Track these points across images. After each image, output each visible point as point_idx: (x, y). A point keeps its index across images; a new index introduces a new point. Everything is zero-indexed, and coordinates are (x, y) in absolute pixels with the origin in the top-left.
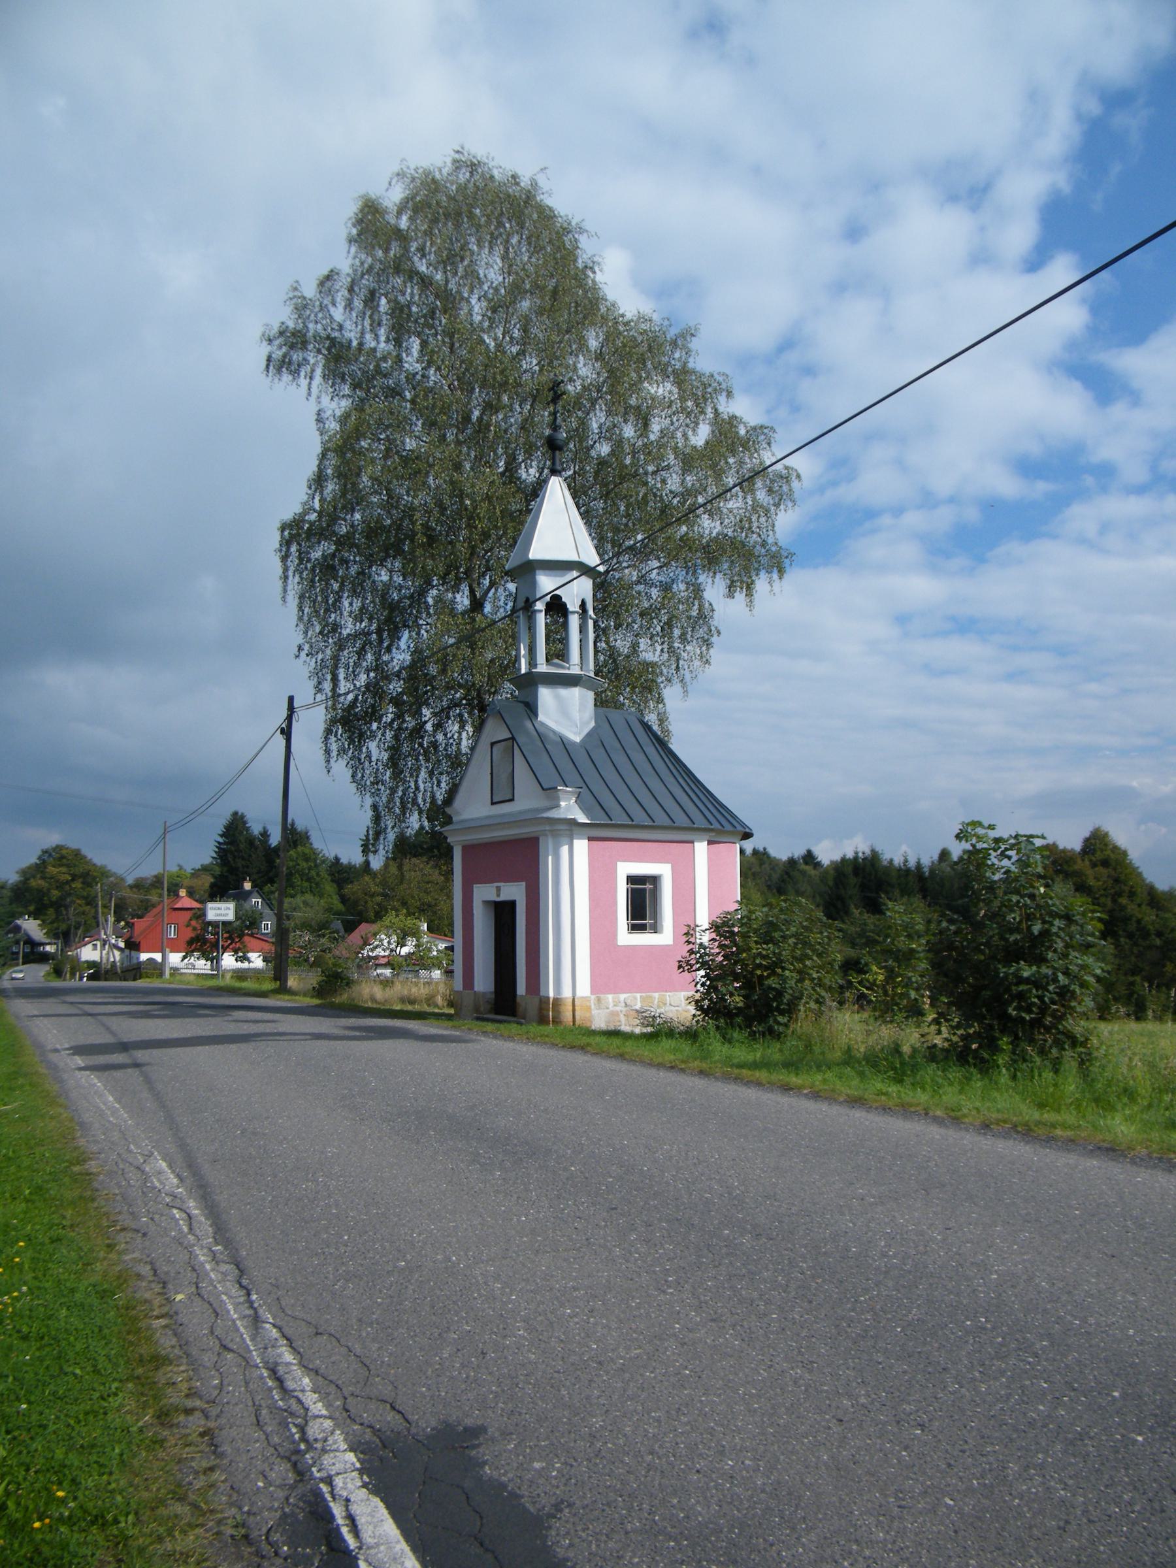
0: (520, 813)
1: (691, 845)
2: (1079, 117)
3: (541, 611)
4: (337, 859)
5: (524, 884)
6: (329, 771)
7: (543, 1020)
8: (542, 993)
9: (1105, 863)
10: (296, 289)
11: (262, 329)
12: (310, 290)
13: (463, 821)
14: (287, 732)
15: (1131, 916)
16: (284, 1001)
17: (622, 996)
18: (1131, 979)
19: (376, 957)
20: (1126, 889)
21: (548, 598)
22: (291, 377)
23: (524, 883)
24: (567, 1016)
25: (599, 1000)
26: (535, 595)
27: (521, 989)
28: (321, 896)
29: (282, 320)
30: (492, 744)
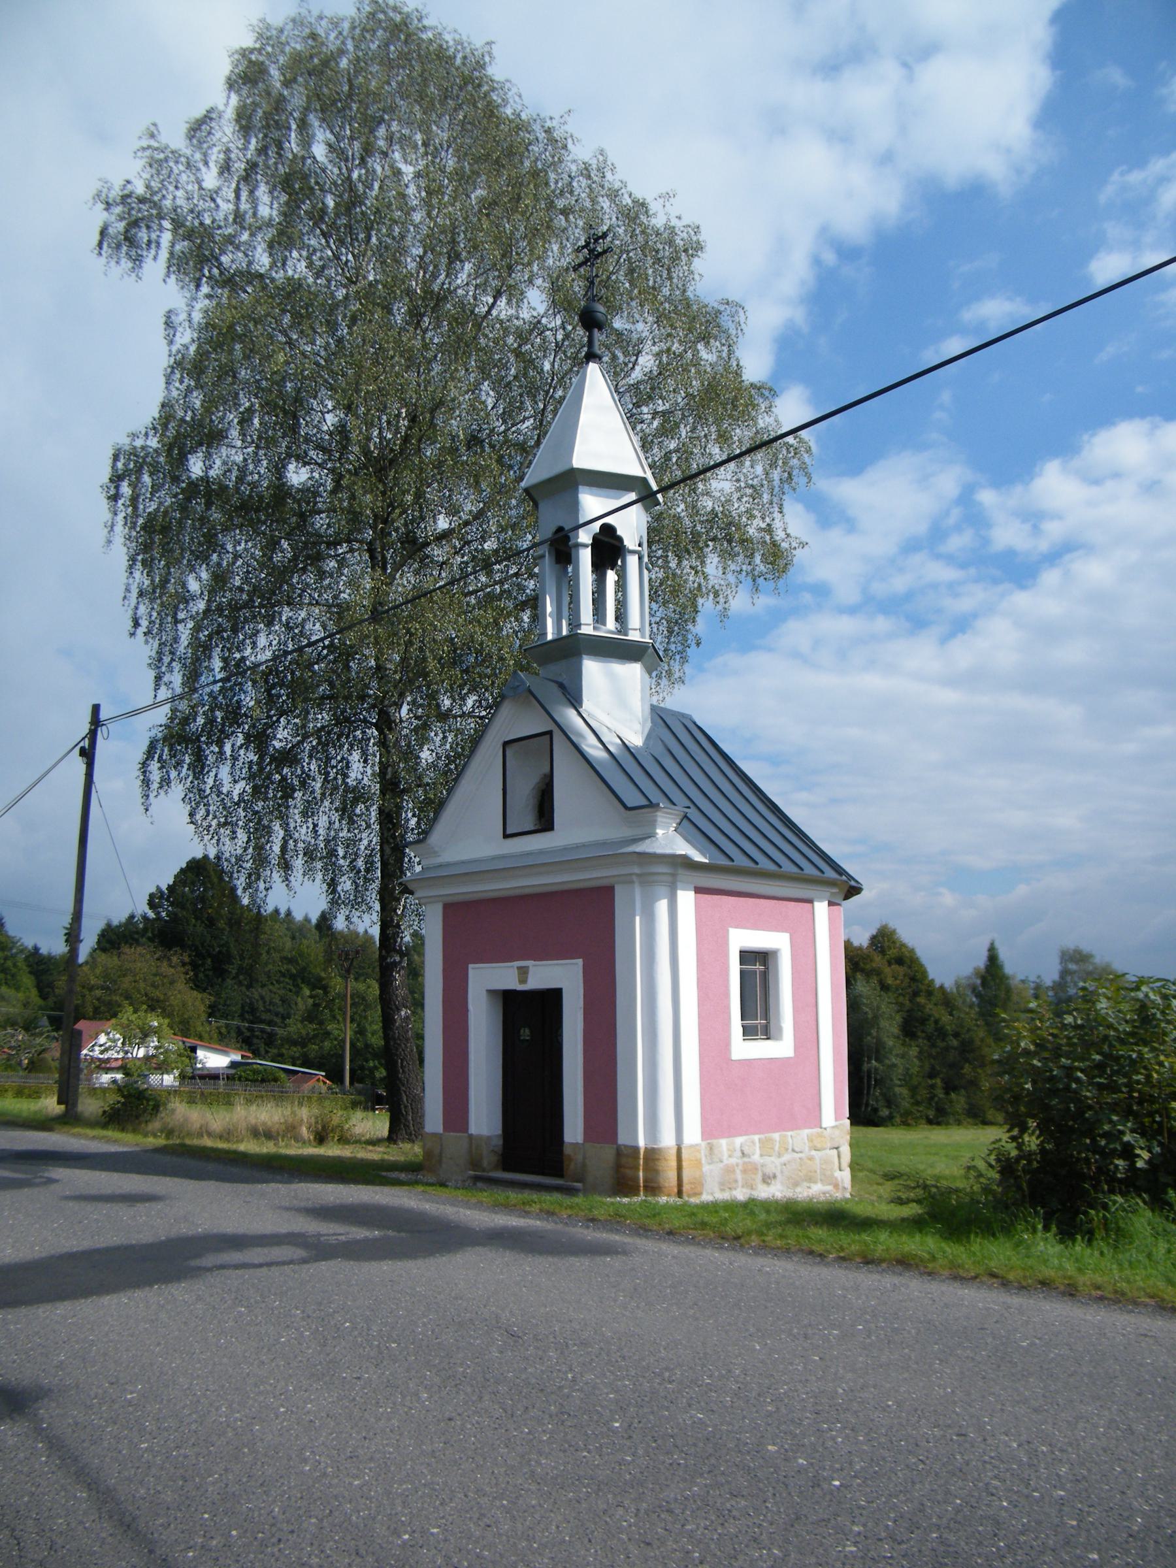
0: (566, 849)
1: (808, 905)
2: (817, 261)
3: (586, 546)
4: (36, 949)
5: (580, 961)
6: (147, 810)
7: (623, 1184)
8: (623, 1139)
9: (900, 961)
10: (152, 136)
11: (99, 185)
12: (175, 138)
13: (440, 866)
14: (88, 755)
15: (930, 1016)
16: (86, 1137)
17: (739, 1141)
18: (930, 1082)
19: (109, 1060)
20: (923, 987)
21: (596, 526)
22: (130, 265)
24: (669, 1176)
25: (711, 1148)
26: (577, 518)
27: (574, 1129)
28: (18, 989)
30: (506, 744)
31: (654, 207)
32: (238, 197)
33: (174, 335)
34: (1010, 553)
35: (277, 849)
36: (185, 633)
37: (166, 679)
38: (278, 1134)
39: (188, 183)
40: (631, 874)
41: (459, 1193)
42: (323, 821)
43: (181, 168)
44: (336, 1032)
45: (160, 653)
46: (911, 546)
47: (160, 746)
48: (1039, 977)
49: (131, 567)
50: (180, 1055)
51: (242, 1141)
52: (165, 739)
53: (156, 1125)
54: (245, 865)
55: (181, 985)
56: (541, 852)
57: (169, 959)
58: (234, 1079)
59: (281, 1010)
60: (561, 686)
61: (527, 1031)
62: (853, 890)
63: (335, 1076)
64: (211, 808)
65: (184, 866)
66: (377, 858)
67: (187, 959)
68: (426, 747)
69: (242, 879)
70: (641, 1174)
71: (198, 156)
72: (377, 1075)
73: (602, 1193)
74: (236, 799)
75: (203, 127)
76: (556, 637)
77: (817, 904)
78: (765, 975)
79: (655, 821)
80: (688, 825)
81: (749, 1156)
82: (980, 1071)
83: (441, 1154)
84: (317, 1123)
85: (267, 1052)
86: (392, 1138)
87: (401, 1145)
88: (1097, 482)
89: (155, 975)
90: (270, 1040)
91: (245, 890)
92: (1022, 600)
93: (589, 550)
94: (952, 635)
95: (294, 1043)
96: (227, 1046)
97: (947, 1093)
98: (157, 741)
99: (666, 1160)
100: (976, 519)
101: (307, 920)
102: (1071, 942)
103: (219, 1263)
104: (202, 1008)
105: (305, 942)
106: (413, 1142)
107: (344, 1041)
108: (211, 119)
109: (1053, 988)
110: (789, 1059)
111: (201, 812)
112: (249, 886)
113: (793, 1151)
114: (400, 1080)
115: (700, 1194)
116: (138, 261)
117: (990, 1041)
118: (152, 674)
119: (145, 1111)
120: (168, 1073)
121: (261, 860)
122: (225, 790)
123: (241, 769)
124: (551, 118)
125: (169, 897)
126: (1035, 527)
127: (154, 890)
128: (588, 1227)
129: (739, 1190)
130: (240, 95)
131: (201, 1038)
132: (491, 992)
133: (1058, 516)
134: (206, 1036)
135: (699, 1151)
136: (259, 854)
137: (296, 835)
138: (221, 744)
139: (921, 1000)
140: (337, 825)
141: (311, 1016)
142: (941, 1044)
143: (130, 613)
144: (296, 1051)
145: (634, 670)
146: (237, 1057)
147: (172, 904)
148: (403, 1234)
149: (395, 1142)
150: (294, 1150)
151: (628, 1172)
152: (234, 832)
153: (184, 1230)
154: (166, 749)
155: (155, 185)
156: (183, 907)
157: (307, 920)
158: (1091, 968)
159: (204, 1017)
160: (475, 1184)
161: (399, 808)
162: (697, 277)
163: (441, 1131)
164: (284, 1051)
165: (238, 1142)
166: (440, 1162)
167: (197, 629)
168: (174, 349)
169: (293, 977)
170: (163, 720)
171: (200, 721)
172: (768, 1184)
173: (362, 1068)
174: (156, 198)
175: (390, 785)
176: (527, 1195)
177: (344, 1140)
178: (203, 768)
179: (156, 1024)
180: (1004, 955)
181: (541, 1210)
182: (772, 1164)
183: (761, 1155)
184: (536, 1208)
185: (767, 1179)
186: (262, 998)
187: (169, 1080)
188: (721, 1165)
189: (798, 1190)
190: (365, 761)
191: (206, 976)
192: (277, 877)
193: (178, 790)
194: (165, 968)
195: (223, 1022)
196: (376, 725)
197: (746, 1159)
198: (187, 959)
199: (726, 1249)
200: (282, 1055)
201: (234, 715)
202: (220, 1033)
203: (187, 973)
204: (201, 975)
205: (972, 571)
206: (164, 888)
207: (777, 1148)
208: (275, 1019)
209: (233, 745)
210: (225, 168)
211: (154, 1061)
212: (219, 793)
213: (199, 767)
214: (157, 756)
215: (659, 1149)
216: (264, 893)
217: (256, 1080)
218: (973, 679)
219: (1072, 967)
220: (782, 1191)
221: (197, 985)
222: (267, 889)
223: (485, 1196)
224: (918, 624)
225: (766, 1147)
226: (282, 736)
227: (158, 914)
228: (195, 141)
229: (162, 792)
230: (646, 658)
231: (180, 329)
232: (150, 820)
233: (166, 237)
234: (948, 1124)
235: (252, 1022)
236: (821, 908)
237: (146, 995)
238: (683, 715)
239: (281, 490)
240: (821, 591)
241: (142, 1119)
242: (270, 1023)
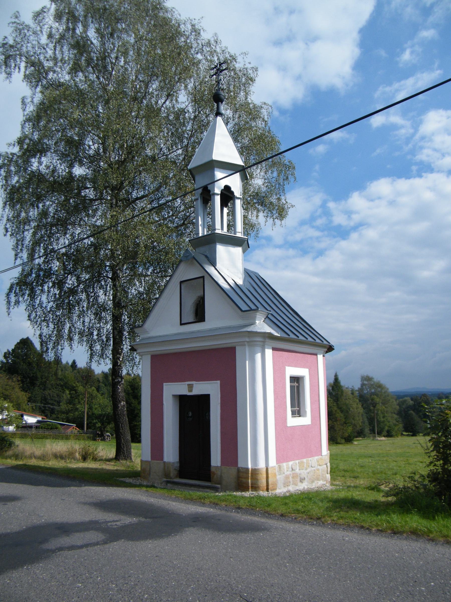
0: (211, 330)
1: (315, 356)
3: (218, 194)
5: (219, 382)
6: (9, 314)
8: (241, 464)
10: (17, 17)
13: (149, 338)
17: (291, 463)
22: (6, 76)
23: (219, 382)
24: (263, 482)
25: (280, 467)
29: (6, 35)
30: (181, 282)
31: (239, 59)
32: (55, 49)
33: (26, 108)
34: (340, 226)
35: (66, 331)
36: (28, 235)
37: (20, 255)
38: (66, 456)
39: (33, 40)
40: (244, 341)
41: (162, 491)
42: (87, 320)
43: (31, 33)
44: (80, 409)
45: (17, 244)
46: (303, 223)
47: (15, 286)
48: (353, 386)
49: (4, 207)
50: (17, 418)
51: (50, 460)
52: (17, 284)
53: (10, 453)
54: (52, 338)
55: (17, 389)
56: (199, 332)
57: (12, 379)
58: (39, 428)
59: (57, 399)
60: (206, 257)
61: (191, 414)
62: (330, 349)
63: (80, 426)
64: (38, 313)
65: (19, 341)
66: (111, 336)
67: (19, 379)
68: (134, 288)
69: (51, 345)
70: (250, 481)
71: (39, 28)
72: (97, 425)
73: (230, 490)
74: (49, 310)
75: (41, 15)
76: (203, 235)
77: (318, 356)
78: (298, 387)
79: (256, 317)
80: (268, 319)
81: (295, 470)
82: (335, 423)
83: (150, 471)
84: (83, 451)
85: (51, 416)
86: (117, 458)
87: (121, 461)
88: (372, 200)
89: (6, 385)
90: (52, 411)
91: (52, 349)
92: (343, 244)
93: (219, 196)
94: (317, 257)
95: (64, 413)
96: (35, 414)
98: (14, 284)
99: (261, 474)
100: (327, 213)
101: (67, 363)
103: (59, 546)
104: (26, 398)
105: (67, 372)
106: (126, 460)
107: (84, 412)
108: (45, 12)
109: (358, 391)
110: (309, 425)
111: (34, 315)
112: (54, 347)
113: (311, 466)
114: (121, 433)
115: (276, 489)
116: (9, 74)
117: (338, 411)
118: (13, 253)
119: (5, 446)
120: (12, 425)
121: (60, 336)
122: (44, 306)
123: (52, 296)
124: (195, 19)
125: (12, 354)
126: (349, 216)
127: (6, 351)
128: (238, 512)
129: (291, 486)
130: (56, 4)
131: (25, 411)
132: (174, 396)
133: (357, 212)
134: (27, 410)
135: (275, 469)
136: (59, 334)
137: (76, 326)
138: (42, 285)
140: (93, 321)
141: (70, 402)
143: (3, 227)
144: (64, 416)
145: (238, 250)
146: (40, 418)
147: (14, 357)
148: (148, 520)
149: (119, 460)
150: (74, 465)
151: (244, 480)
152: (48, 324)
153: (35, 521)
154: (18, 288)
155: (18, 40)
156: (18, 358)
157: (67, 363)
158: (372, 383)
159: (26, 402)
160: (167, 485)
161: (122, 314)
162: (252, 93)
164: (59, 416)
165: (48, 461)
166: (149, 474)
167: (34, 234)
168: (26, 113)
169: (62, 386)
170: (17, 275)
171: (34, 275)
172: (302, 482)
173: (91, 423)
174: (19, 46)
175: (117, 304)
177: (95, 459)
178: (34, 296)
179: (7, 405)
180: (340, 378)
181: (211, 502)
182: (304, 473)
183: (299, 470)
184: (207, 501)
185: (302, 480)
186: (49, 394)
187: (11, 428)
188: (284, 475)
189: (314, 484)
190: (105, 295)
191: (27, 385)
192: (66, 344)
193: (23, 306)
194: (10, 382)
195: (34, 404)
196: (111, 278)
197: (293, 472)
198: (19, 379)
199: (316, 525)
200: (58, 418)
201: (48, 273)
202: (33, 409)
203: (19, 385)
204: (25, 385)
205: (326, 233)
206: (10, 350)
207: (305, 466)
208: (54, 403)
209: (48, 287)
210: (50, 36)
211: (6, 421)
212: (42, 307)
213: (32, 296)
214: (13, 291)
215: (258, 469)
216: (61, 351)
217: (49, 428)
218: (325, 273)
219: (366, 382)
220: (307, 485)
221: (24, 389)
222: (62, 349)
223: (177, 492)
224: (304, 252)
225: (301, 464)
226: (71, 281)
227: (7, 361)
228: (37, 21)
229: (16, 307)
230: (244, 245)
231: (28, 105)
232: (10, 319)
233: (23, 65)
235: (45, 404)
236: (320, 357)
237: (3, 393)
238: (255, 273)
239: (71, 177)
240: (269, 239)
241: (4, 450)
242: (52, 404)
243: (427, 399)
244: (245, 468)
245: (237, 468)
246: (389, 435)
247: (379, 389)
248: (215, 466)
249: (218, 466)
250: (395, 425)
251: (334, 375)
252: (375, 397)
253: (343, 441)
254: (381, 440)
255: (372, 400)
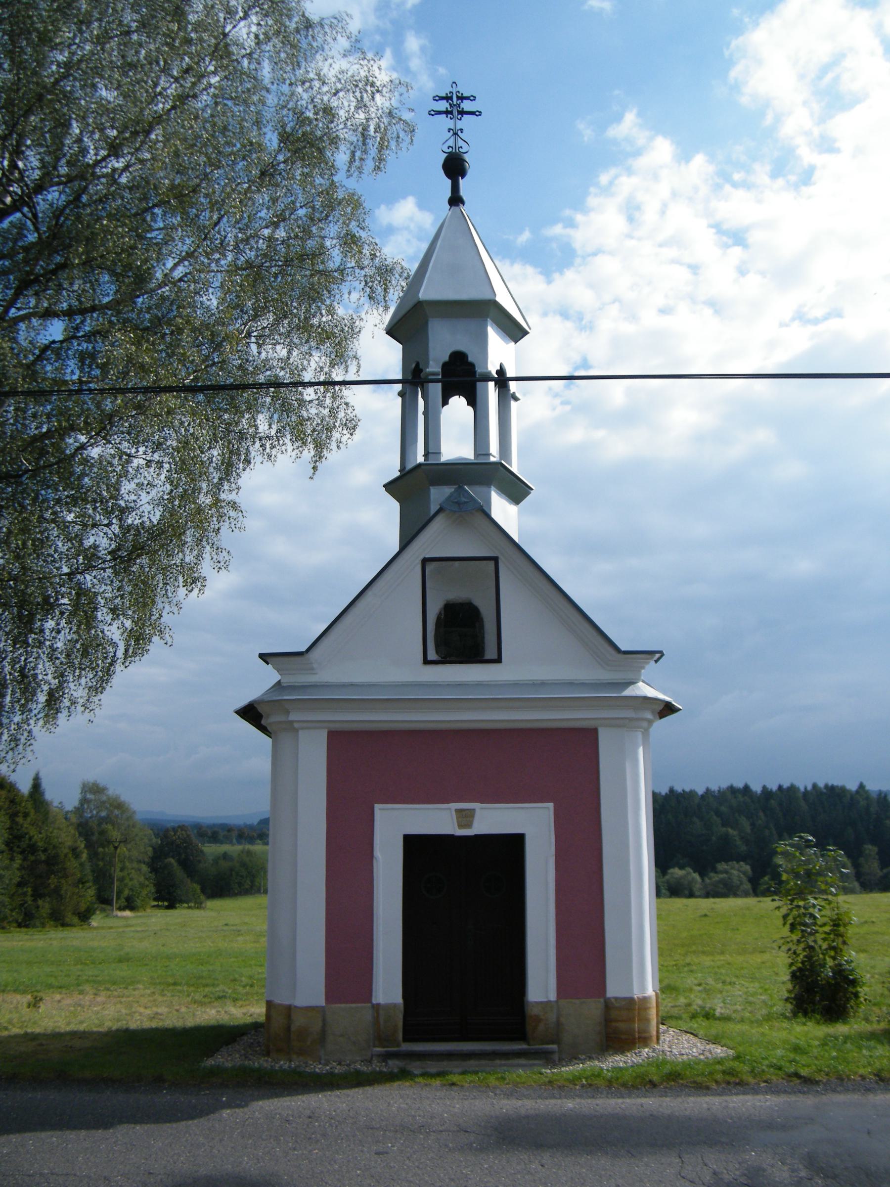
0: (516, 685)
5: (551, 805)
8: (614, 990)
13: (304, 687)
30: (425, 561)
56: (479, 685)
97: (35, 900)
102: (92, 776)
139: (20, 820)
142: (32, 858)
158: (104, 798)
163: (324, 1004)
176: (444, 1065)
180: (45, 784)
219: (89, 796)
234: (34, 926)
243: (188, 836)
244: (625, 999)
245: (602, 1000)
246: (130, 905)
247: (116, 812)
248: (541, 1003)
249: (549, 1002)
250: (142, 886)
251: (32, 775)
252: (110, 827)
253: (76, 920)
254: (122, 917)
255: (102, 833)
